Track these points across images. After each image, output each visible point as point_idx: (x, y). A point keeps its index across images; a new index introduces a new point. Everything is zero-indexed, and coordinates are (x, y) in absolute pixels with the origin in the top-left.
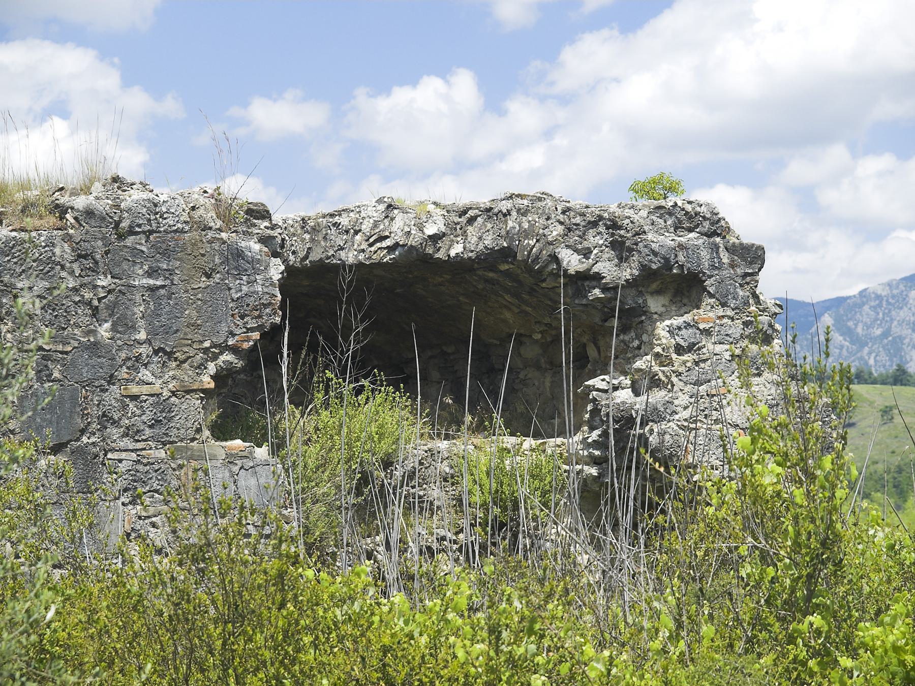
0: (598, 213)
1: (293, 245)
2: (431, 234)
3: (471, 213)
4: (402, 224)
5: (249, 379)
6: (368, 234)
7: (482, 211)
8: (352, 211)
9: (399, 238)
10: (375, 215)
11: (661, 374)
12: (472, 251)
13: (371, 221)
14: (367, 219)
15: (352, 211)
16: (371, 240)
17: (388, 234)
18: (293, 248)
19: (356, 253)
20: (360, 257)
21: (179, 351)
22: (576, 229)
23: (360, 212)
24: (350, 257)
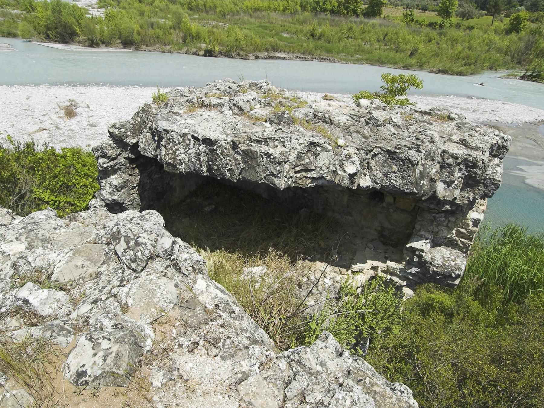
0: (465, 157)
1: (228, 164)
2: (351, 173)
3: (375, 151)
4: (327, 162)
5: (160, 175)
6: (294, 163)
7: (384, 151)
8: (277, 140)
9: (324, 172)
10: (299, 147)
11: (459, 242)
12: (377, 184)
13: (296, 152)
14: (292, 151)
15: (277, 140)
16: (297, 169)
17: (314, 168)
18: (229, 167)
19: (286, 179)
20: (289, 183)
21: (150, 41)
22: (447, 167)
23: (284, 142)
24: (282, 183)
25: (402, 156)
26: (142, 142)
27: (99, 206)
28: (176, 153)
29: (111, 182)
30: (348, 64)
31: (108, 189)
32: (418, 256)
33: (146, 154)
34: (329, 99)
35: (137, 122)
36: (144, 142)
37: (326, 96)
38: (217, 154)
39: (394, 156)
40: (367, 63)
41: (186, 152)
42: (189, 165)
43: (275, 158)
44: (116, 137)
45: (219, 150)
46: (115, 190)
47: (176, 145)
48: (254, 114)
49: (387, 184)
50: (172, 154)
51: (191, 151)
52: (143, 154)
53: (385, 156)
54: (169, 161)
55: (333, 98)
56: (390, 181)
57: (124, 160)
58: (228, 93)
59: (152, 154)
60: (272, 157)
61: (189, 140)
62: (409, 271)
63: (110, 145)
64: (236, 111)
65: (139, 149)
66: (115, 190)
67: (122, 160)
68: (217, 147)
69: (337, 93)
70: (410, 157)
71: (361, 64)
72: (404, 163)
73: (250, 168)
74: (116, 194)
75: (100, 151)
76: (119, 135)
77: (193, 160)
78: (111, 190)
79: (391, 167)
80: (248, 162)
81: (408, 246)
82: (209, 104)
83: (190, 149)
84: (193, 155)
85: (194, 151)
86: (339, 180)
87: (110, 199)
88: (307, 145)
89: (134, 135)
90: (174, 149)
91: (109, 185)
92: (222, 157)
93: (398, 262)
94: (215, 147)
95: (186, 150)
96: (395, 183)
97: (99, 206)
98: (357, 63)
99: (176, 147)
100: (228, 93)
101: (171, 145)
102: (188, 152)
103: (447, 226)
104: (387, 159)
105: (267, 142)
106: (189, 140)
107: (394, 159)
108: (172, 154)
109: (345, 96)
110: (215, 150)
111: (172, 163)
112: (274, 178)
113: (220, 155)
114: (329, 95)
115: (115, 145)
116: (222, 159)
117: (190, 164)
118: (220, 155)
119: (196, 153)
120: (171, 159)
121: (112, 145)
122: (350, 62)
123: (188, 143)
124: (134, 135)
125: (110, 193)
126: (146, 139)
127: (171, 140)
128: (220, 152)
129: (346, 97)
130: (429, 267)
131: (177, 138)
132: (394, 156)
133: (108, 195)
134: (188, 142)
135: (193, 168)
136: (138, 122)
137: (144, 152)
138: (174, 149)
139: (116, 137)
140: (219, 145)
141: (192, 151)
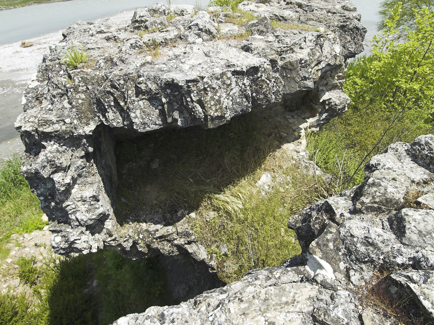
25: (351, 26)
26: (136, 117)
27: (78, 236)
28: (220, 101)
29: (82, 197)
30: (17, 8)
31: (83, 207)
32: (328, 105)
33: (148, 128)
34: (28, 45)
35: (80, 101)
36: (139, 115)
37: (23, 44)
38: (263, 81)
39: (346, 29)
40: (35, 3)
41: (228, 94)
42: (234, 109)
43: (306, 61)
44: (66, 134)
45: (264, 75)
46: (92, 203)
47: (217, 92)
48: (228, 32)
49: (346, 53)
50: (215, 105)
51: (234, 91)
52: (144, 131)
53: (339, 32)
54: (216, 114)
55: (32, 44)
56: (348, 50)
57: (81, 160)
58: (159, 24)
59: (156, 124)
60: (303, 62)
61: (229, 78)
62: (322, 119)
63: (58, 151)
64: (206, 37)
65: (135, 127)
66: (92, 203)
67: (80, 162)
68: (261, 73)
69: (27, 39)
70: (357, 25)
71: (29, 5)
72: (353, 32)
73: (290, 82)
74: (97, 206)
75: (48, 167)
76: (68, 129)
77: (238, 100)
78: (87, 206)
79: (346, 39)
80: (286, 76)
81: (321, 101)
82: (164, 41)
83: (232, 89)
84: (237, 94)
85: (237, 89)
86: (340, 61)
87: (94, 217)
88: (315, 39)
89: (84, 121)
90: (217, 98)
91: (80, 202)
92: (268, 82)
93: (313, 116)
94: (259, 74)
95: (228, 93)
96: (351, 49)
97: (78, 236)
98: (25, 5)
99: (218, 94)
100: (159, 24)
101: (210, 94)
102: (231, 93)
103: (331, 76)
104: (341, 33)
105: (292, 49)
106: (229, 78)
107: (346, 31)
108: (215, 105)
109: (41, 38)
110: (258, 78)
111: (219, 115)
112: (305, 82)
113: (266, 80)
114: (26, 41)
115: (64, 147)
116: (268, 84)
117: (235, 106)
118: (266, 80)
119: (240, 90)
120: (216, 111)
121: (60, 149)
122: (18, 5)
123: (229, 83)
124: (84, 121)
125: (88, 211)
126: (141, 109)
127: (208, 89)
128: (266, 76)
129: (43, 39)
130: (336, 108)
131: (215, 84)
132: (346, 29)
133: (87, 214)
134: (228, 82)
135: (239, 110)
136: (83, 99)
137: (144, 128)
138: (217, 98)
139: (66, 134)
140: (263, 69)
141: (236, 90)
